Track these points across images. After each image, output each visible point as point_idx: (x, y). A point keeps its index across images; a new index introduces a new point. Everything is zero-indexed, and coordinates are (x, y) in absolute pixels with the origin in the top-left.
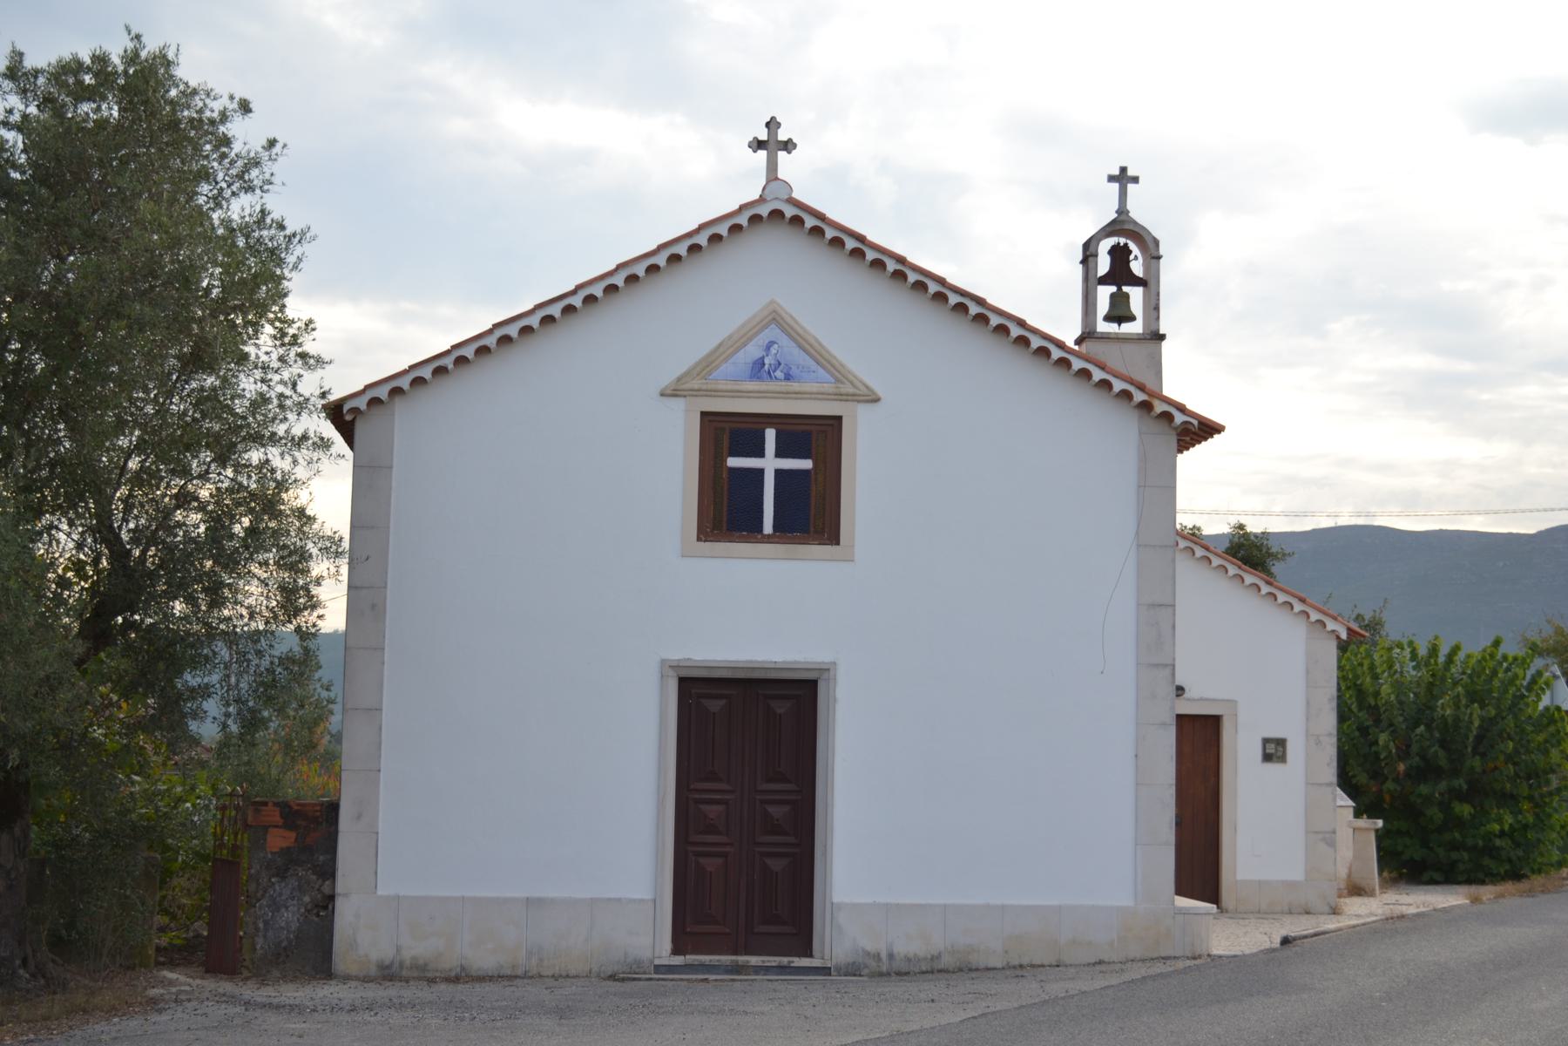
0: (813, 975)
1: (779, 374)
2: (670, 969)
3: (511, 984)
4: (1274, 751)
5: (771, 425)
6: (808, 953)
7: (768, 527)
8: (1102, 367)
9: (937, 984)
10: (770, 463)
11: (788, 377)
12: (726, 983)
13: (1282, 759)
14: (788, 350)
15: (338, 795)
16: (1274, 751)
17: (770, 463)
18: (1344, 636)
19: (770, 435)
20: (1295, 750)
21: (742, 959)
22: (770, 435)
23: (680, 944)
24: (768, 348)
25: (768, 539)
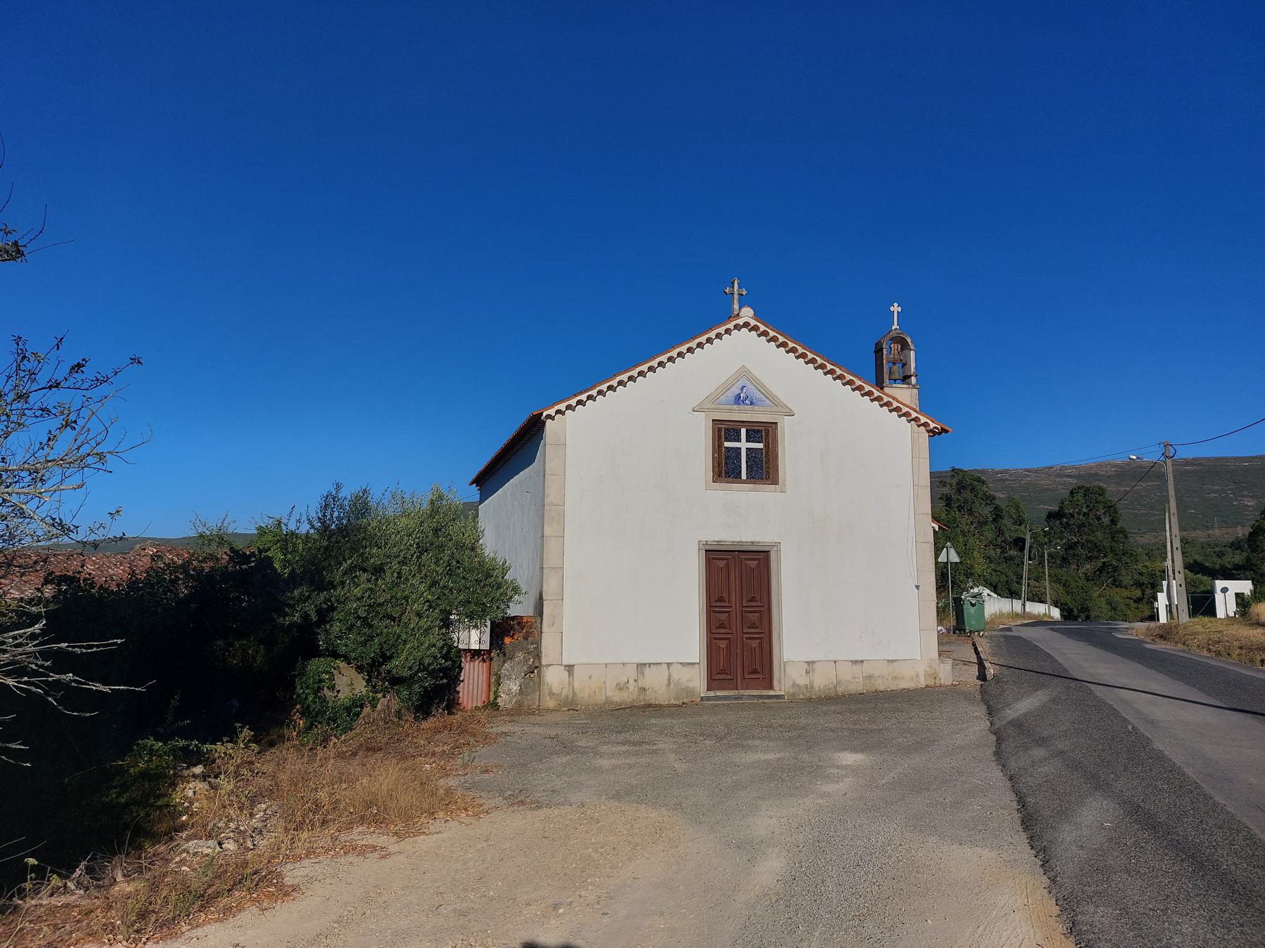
1: (747, 402)
2: (708, 699)
6: (771, 687)
7: (744, 476)
8: (898, 401)
9: (1083, 854)
10: (744, 445)
11: (752, 403)
12: (539, 531)
14: (751, 389)
17: (744, 445)
19: (743, 431)
21: (742, 692)
22: (743, 431)
23: (712, 683)
24: (742, 390)
25: (744, 482)
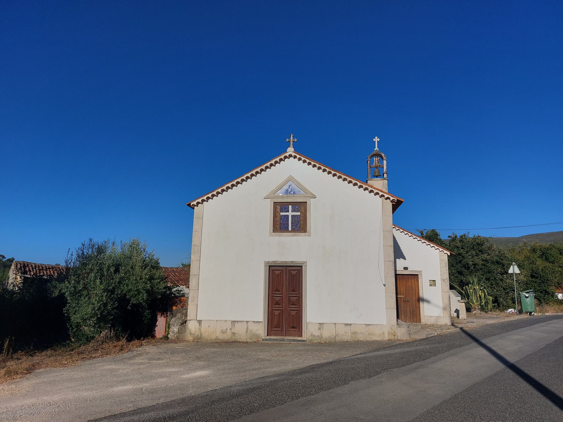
0: (274, 335)
1: (292, 193)
3: (417, 301)
4: (433, 283)
5: (290, 205)
7: (290, 229)
10: (290, 214)
13: (435, 285)
15: (275, 205)
16: (433, 283)
18: (449, 255)
20: (438, 283)
24: (289, 187)
25: (290, 232)
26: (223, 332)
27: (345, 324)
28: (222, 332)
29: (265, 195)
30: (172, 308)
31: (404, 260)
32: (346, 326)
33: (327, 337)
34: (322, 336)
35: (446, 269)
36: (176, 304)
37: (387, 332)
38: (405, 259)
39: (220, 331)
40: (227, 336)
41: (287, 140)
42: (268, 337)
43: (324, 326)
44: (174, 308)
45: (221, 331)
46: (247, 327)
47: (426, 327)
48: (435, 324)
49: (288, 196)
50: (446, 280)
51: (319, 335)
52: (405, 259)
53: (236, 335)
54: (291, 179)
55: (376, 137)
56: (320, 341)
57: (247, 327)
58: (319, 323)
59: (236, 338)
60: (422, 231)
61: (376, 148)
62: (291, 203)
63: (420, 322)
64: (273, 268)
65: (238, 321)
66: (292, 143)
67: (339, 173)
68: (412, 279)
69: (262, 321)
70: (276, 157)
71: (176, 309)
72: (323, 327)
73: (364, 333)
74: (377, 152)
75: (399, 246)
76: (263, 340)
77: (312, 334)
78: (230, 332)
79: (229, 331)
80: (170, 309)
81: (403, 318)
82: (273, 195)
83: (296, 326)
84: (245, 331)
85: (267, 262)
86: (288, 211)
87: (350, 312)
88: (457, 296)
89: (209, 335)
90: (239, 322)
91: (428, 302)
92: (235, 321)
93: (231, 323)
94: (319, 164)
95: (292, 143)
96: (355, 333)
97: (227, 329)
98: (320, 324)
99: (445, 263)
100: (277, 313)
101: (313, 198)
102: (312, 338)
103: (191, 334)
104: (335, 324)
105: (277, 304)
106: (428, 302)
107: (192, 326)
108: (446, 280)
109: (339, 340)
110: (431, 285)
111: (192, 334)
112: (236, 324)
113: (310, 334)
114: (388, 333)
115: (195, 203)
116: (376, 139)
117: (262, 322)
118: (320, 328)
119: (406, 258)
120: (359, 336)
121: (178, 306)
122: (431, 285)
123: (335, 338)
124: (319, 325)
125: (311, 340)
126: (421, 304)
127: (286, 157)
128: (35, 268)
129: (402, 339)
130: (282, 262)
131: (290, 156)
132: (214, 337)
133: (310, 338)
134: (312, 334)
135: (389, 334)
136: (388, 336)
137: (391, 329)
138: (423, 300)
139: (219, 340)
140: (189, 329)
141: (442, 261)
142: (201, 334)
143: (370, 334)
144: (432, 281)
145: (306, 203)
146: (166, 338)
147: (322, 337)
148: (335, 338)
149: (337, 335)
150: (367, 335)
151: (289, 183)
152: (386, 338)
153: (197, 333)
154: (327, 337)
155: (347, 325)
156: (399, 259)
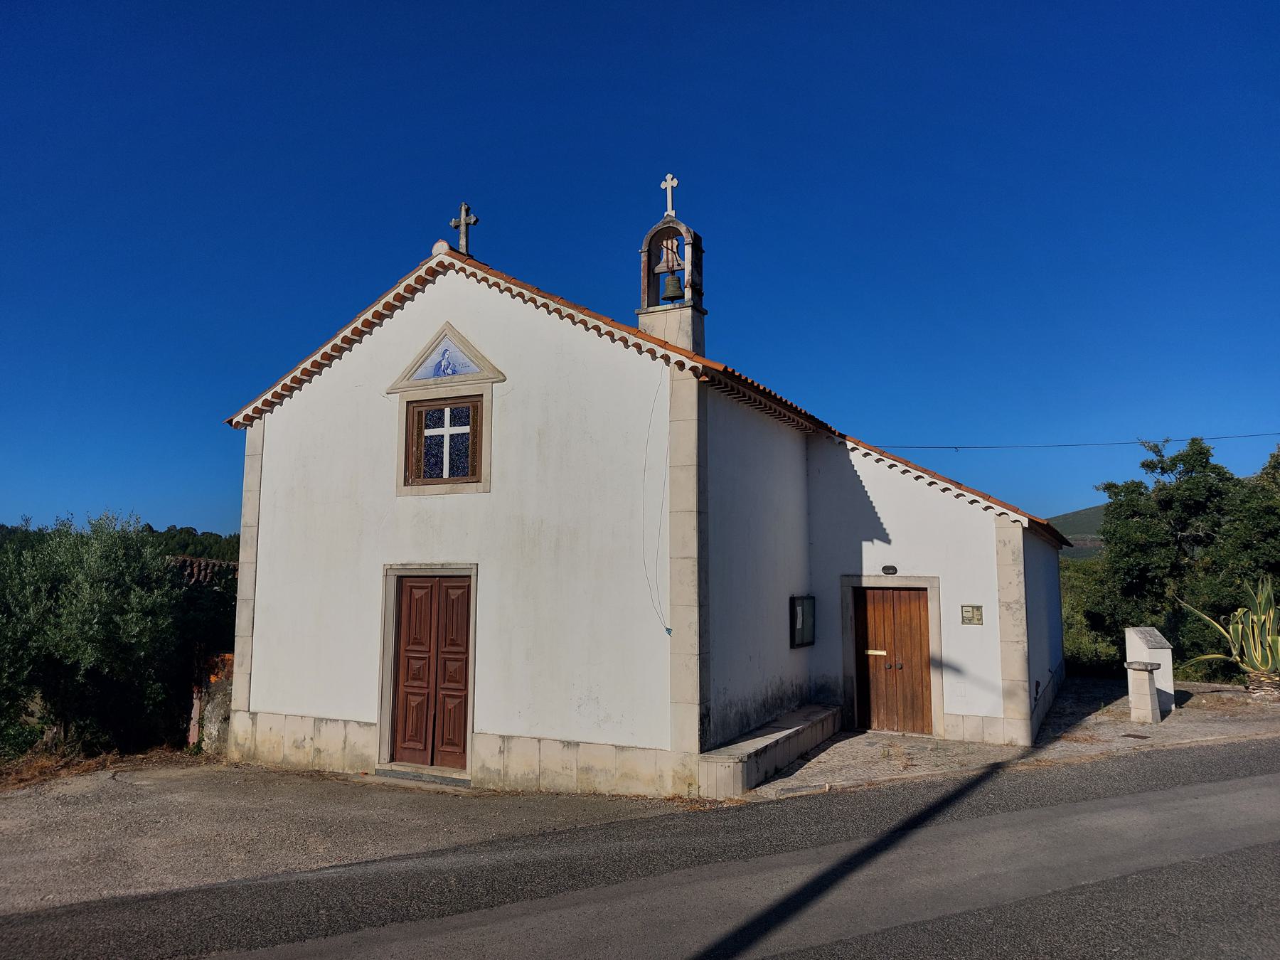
1: (449, 371)
4: (973, 615)
7: (446, 474)
16: (973, 615)
18: (1026, 525)
20: (991, 614)
26: (298, 745)
27: (562, 742)
28: (295, 745)
29: (388, 385)
30: (209, 678)
31: (885, 545)
32: (566, 748)
33: (519, 776)
34: (508, 771)
35: (1016, 572)
36: (216, 671)
37: (672, 773)
38: (888, 542)
39: (292, 742)
40: (301, 758)
41: (452, 224)
42: (396, 767)
43: (513, 743)
44: (213, 679)
45: (294, 742)
46: (346, 737)
47: (942, 747)
48: (977, 739)
49: (438, 382)
50: (1015, 606)
51: (500, 771)
52: (888, 542)
53: (322, 755)
54: (447, 331)
55: (669, 177)
56: (501, 784)
57: (346, 737)
58: (500, 736)
59: (322, 762)
60: (1156, 446)
61: (670, 212)
62: (449, 402)
63: (931, 734)
64: (408, 583)
65: (327, 720)
66: (463, 229)
67: (554, 302)
68: (912, 603)
69: (375, 722)
70: (407, 273)
71: (216, 681)
72: (511, 748)
73: (610, 771)
74: (665, 224)
75: (872, 502)
76: (377, 772)
77: (483, 766)
78: (311, 746)
79: (308, 743)
80: (206, 680)
81: (882, 717)
82: (405, 383)
83: (456, 741)
84: (341, 745)
85: (389, 567)
86: (453, 424)
87: (579, 707)
88: (1158, 646)
89: (271, 749)
90: (329, 721)
91: (956, 670)
92: (321, 720)
93: (313, 721)
94: (506, 282)
95: (463, 229)
96: (588, 770)
97: (305, 739)
98: (502, 737)
99: (1013, 553)
100: (414, 701)
101: (497, 382)
102: (483, 776)
103: (237, 744)
104: (539, 740)
105: (416, 677)
106: (956, 670)
107: (239, 724)
108: (1015, 606)
109: (548, 786)
110: (965, 621)
111: (238, 744)
112: (324, 727)
113: (480, 764)
114: (674, 776)
115: (239, 418)
116: (669, 183)
117: (375, 724)
118: (502, 749)
119: (890, 537)
120: (597, 780)
121: (220, 674)
122: (965, 621)
123: (538, 779)
124: (500, 742)
125: (481, 781)
126: (934, 677)
127: (433, 273)
128: (206, 570)
129: (712, 796)
130: (421, 565)
131: (444, 268)
132: (279, 757)
133: (480, 776)
134: (483, 766)
135: (678, 781)
136: (674, 783)
137: (683, 764)
138: (940, 665)
139: (289, 763)
140: (234, 733)
141: (1005, 544)
142: (256, 746)
143: (625, 776)
144: (970, 609)
145: (479, 399)
146: (198, 746)
147: (506, 774)
148: (538, 779)
149: (542, 773)
150: (617, 776)
151: (443, 343)
152: (669, 790)
153: (248, 744)
154: (519, 776)
155: (567, 744)
156: (870, 543)
